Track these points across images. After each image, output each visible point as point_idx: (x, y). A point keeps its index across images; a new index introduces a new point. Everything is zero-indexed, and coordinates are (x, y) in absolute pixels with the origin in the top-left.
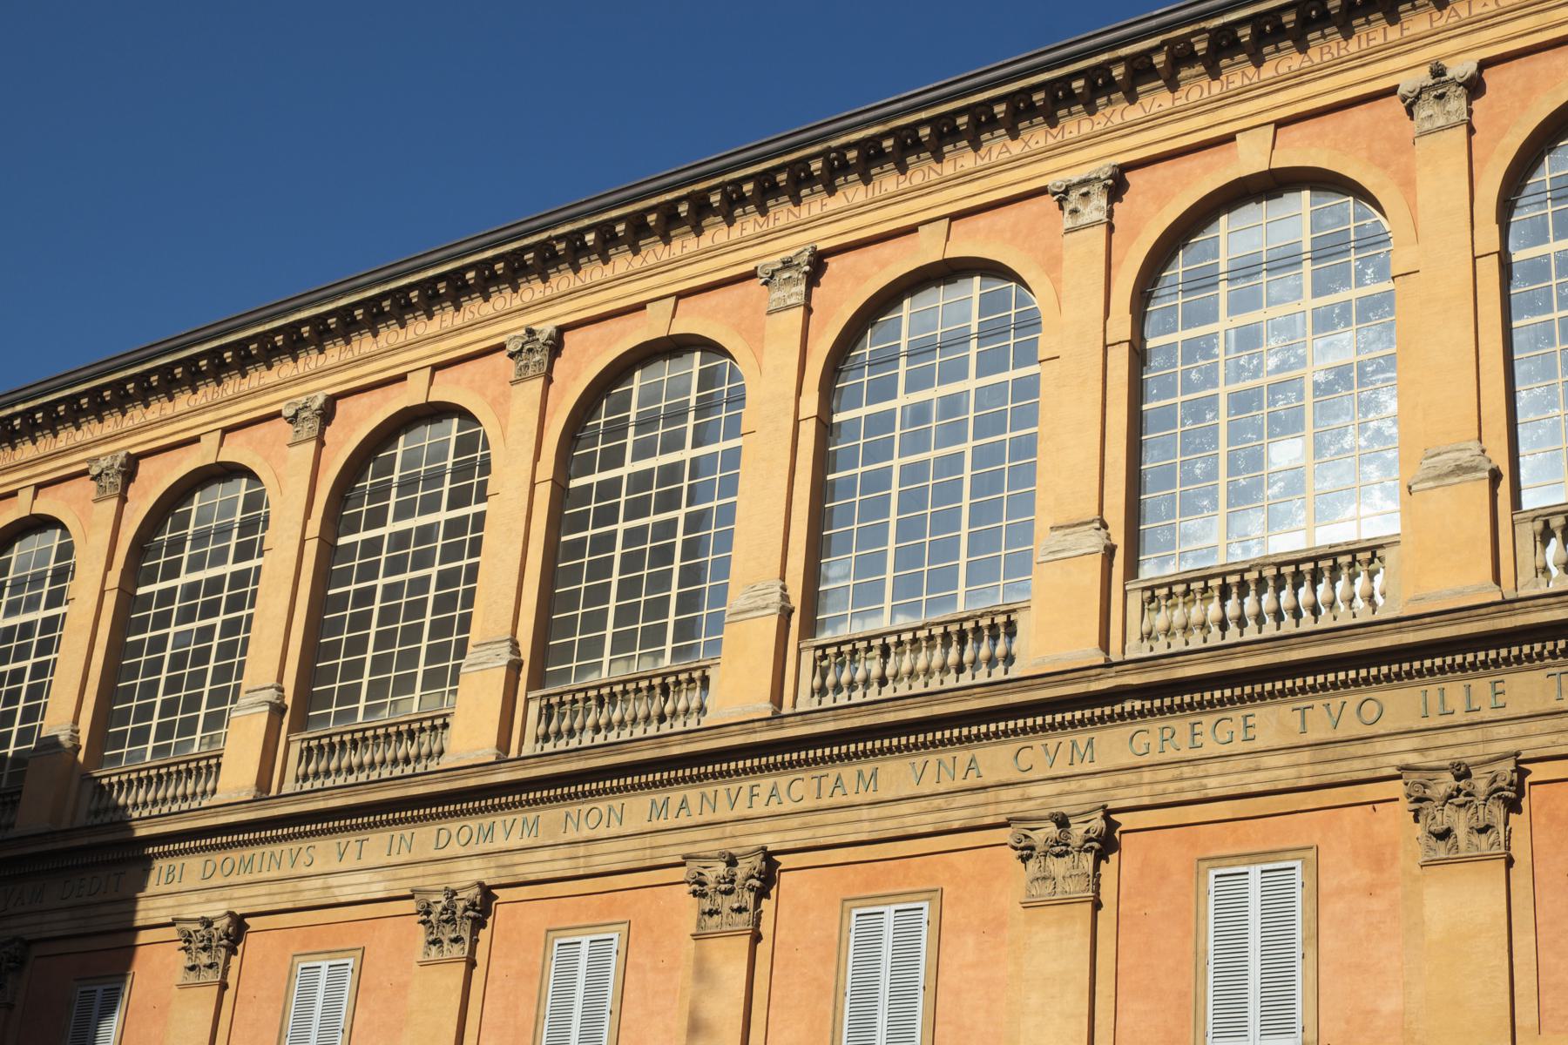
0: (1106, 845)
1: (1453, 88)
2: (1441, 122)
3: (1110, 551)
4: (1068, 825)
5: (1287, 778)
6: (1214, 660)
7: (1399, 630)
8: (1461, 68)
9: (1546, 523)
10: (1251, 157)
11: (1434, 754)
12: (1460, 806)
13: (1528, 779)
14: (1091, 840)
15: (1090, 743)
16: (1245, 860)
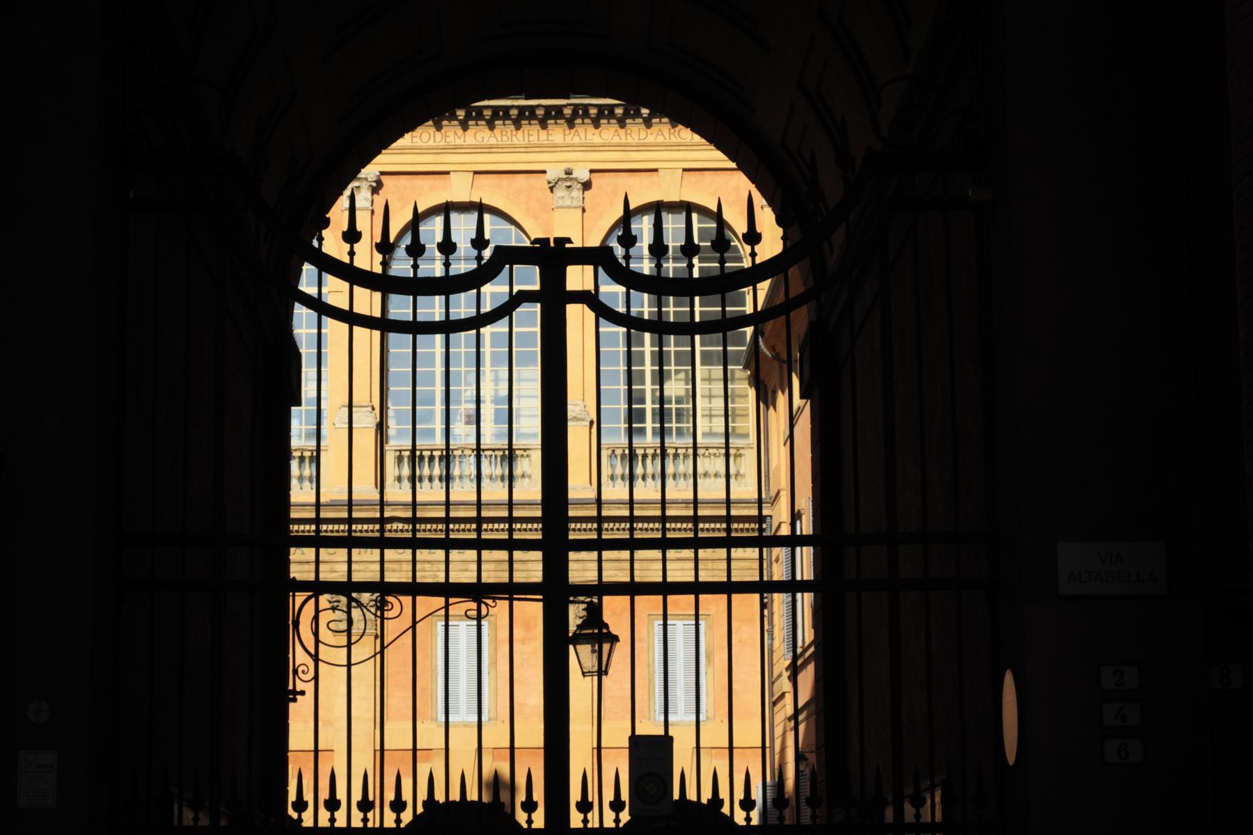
2: (568, 202)
8: (583, 175)
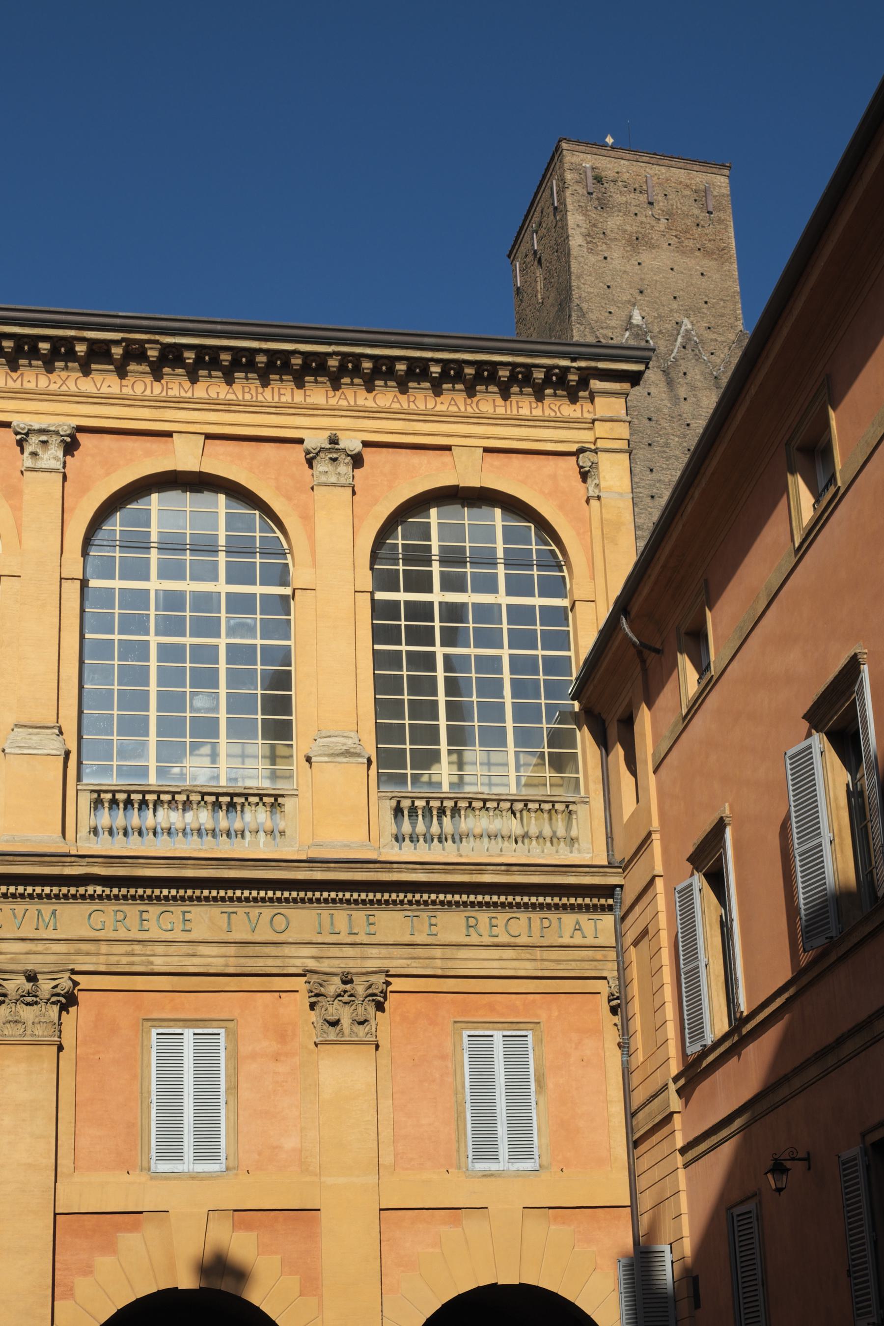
0: (68, 1001)
1: (343, 456)
2: (333, 479)
3: (67, 754)
4: (37, 980)
5: (217, 965)
6: (169, 866)
7: (311, 869)
8: (351, 443)
9: (399, 802)
10: (185, 456)
11: (326, 962)
12: (346, 1003)
13: (390, 988)
14: (58, 995)
15: (54, 912)
16: (181, 1023)
